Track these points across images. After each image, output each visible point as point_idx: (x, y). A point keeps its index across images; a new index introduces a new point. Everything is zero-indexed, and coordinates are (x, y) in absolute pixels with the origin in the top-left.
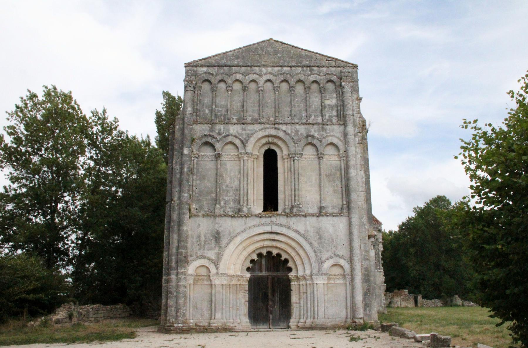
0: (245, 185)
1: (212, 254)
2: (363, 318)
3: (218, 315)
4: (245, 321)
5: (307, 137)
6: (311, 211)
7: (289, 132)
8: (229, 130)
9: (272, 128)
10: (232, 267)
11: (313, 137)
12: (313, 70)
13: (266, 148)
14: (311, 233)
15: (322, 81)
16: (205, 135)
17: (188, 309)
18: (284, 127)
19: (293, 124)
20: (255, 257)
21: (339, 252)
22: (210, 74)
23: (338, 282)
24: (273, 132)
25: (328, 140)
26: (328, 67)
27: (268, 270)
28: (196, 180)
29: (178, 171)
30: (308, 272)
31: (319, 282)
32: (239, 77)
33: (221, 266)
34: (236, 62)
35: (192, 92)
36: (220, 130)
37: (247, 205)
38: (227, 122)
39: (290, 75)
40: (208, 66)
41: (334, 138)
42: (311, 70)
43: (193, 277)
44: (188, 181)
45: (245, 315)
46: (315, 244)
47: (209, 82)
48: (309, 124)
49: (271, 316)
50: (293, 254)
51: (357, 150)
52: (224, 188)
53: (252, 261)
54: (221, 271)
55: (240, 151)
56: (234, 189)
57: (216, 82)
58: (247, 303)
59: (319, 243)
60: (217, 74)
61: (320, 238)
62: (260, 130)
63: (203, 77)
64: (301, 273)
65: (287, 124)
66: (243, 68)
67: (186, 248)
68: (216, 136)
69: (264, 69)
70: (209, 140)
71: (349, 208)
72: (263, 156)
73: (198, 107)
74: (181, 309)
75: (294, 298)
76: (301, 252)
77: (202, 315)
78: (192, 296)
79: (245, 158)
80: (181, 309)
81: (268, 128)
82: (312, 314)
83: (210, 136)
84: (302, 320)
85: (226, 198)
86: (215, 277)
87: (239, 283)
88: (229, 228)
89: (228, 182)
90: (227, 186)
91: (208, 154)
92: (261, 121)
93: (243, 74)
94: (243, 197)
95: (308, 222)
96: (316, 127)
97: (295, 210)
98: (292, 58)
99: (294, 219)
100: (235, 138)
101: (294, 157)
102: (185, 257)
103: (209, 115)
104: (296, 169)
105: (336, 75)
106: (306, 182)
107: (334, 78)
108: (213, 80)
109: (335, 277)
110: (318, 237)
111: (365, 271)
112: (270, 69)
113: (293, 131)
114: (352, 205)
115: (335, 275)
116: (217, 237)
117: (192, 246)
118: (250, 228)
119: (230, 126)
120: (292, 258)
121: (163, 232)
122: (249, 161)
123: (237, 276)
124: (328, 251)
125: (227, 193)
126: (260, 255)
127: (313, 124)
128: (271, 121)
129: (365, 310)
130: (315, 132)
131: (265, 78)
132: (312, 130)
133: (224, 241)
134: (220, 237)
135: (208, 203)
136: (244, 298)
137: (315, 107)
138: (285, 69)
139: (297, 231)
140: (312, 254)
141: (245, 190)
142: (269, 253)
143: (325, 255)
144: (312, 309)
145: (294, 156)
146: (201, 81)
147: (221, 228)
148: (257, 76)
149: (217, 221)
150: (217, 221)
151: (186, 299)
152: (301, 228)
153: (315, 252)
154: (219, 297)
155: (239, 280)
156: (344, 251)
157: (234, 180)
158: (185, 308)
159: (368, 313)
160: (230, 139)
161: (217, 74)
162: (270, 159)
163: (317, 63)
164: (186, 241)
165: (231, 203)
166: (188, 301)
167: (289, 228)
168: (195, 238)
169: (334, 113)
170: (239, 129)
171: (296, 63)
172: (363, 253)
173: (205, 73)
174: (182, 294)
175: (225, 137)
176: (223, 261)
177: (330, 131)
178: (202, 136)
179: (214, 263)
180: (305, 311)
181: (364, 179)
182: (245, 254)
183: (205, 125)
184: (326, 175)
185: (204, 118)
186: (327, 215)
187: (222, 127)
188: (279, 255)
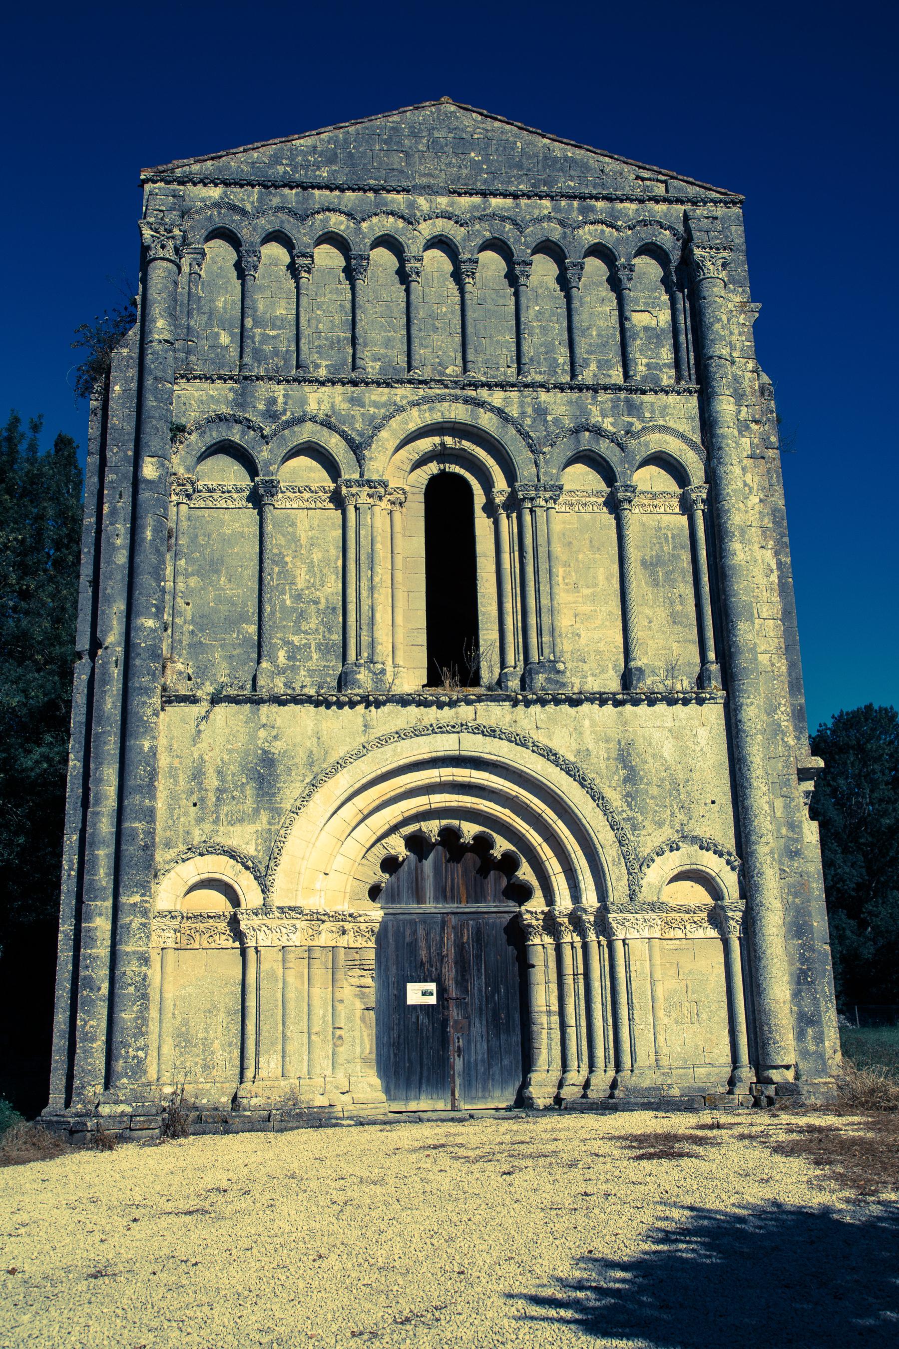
0: (364, 593)
1: (245, 838)
2: (796, 1066)
3: (270, 1065)
4: (367, 1087)
5: (576, 431)
6: (593, 685)
7: (514, 412)
8: (304, 402)
9: (456, 398)
11: (598, 432)
12: (592, 209)
13: (433, 468)
14: (601, 766)
15: (622, 249)
16: (221, 418)
17: (154, 1046)
18: (497, 398)
19: (527, 386)
20: (397, 846)
21: (703, 830)
22: (233, 208)
23: (700, 933)
24: (458, 412)
25: (647, 444)
26: (641, 201)
27: (443, 894)
28: (187, 576)
29: (119, 542)
31: (633, 934)
32: (338, 223)
33: (280, 879)
34: (324, 173)
35: (170, 265)
36: (273, 401)
37: (371, 661)
38: (300, 374)
39: (515, 223)
40: (227, 184)
41: (668, 438)
42: (583, 211)
44: (159, 576)
47: (233, 239)
48: (580, 388)
49: (458, 1064)
51: (749, 478)
52: (288, 602)
53: (390, 864)
54: (278, 899)
55: (345, 476)
56: (322, 606)
57: (257, 239)
59: (628, 795)
60: (260, 212)
61: (631, 777)
62: (414, 404)
63: (210, 218)
64: (564, 903)
65: (502, 386)
66: (349, 194)
67: (150, 815)
68: (256, 419)
69: (422, 201)
70: (236, 435)
71: (729, 680)
72: (422, 498)
73: (192, 323)
74: (126, 1045)
78: (168, 996)
79: (363, 497)
80: (126, 1045)
81: (442, 399)
83: (237, 421)
84: (576, 1077)
85: (296, 639)
86: (256, 921)
87: (343, 941)
88: (308, 744)
89: (301, 583)
90: (298, 597)
91: (229, 484)
92: (417, 374)
93: (350, 215)
94: (358, 636)
95: (587, 723)
96: (602, 397)
97: (540, 679)
98: (520, 166)
100: (326, 431)
101: (532, 499)
102: (146, 848)
103: (234, 353)
104: (542, 540)
105: (670, 228)
106: (576, 586)
107: (665, 238)
108: (245, 233)
109: (687, 916)
110: (623, 772)
111: (796, 895)
112: (443, 201)
113: (529, 410)
114: (743, 661)
116: (264, 773)
117: (171, 809)
118: (382, 741)
119: (307, 388)
121: (66, 761)
122: (377, 509)
124: (660, 824)
125: (297, 622)
126: (416, 843)
127: (594, 389)
128: (447, 375)
129: (800, 1036)
130: (604, 415)
131: (426, 230)
132: (595, 410)
133: (290, 791)
135: (231, 657)
136: (362, 996)
137: (599, 335)
138: (496, 202)
141: (365, 608)
142: (450, 836)
143: (650, 839)
145: (533, 493)
146: (204, 233)
147: (278, 743)
148: (401, 224)
150: (264, 720)
151: (145, 1008)
152: (563, 743)
154: (271, 994)
156: (721, 830)
157: (323, 575)
158: (141, 1043)
159: (812, 1048)
160: (307, 432)
161: (260, 212)
162: (448, 515)
163: (603, 185)
164: (150, 790)
165: (315, 656)
166: (153, 1013)
167: (521, 742)
168: (182, 778)
169: (666, 354)
170: (338, 399)
171: (533, 185)
172: (784, 831)
173: (217, 205)
174: (131, 989)
175: (289, 424)
177: (653, 412)
178: (209, 421)
181: (774, 578)
182: (366, 834)
183: (219, 384)
184: (644, 563)
185: (213, 362)
187: (279, 391)
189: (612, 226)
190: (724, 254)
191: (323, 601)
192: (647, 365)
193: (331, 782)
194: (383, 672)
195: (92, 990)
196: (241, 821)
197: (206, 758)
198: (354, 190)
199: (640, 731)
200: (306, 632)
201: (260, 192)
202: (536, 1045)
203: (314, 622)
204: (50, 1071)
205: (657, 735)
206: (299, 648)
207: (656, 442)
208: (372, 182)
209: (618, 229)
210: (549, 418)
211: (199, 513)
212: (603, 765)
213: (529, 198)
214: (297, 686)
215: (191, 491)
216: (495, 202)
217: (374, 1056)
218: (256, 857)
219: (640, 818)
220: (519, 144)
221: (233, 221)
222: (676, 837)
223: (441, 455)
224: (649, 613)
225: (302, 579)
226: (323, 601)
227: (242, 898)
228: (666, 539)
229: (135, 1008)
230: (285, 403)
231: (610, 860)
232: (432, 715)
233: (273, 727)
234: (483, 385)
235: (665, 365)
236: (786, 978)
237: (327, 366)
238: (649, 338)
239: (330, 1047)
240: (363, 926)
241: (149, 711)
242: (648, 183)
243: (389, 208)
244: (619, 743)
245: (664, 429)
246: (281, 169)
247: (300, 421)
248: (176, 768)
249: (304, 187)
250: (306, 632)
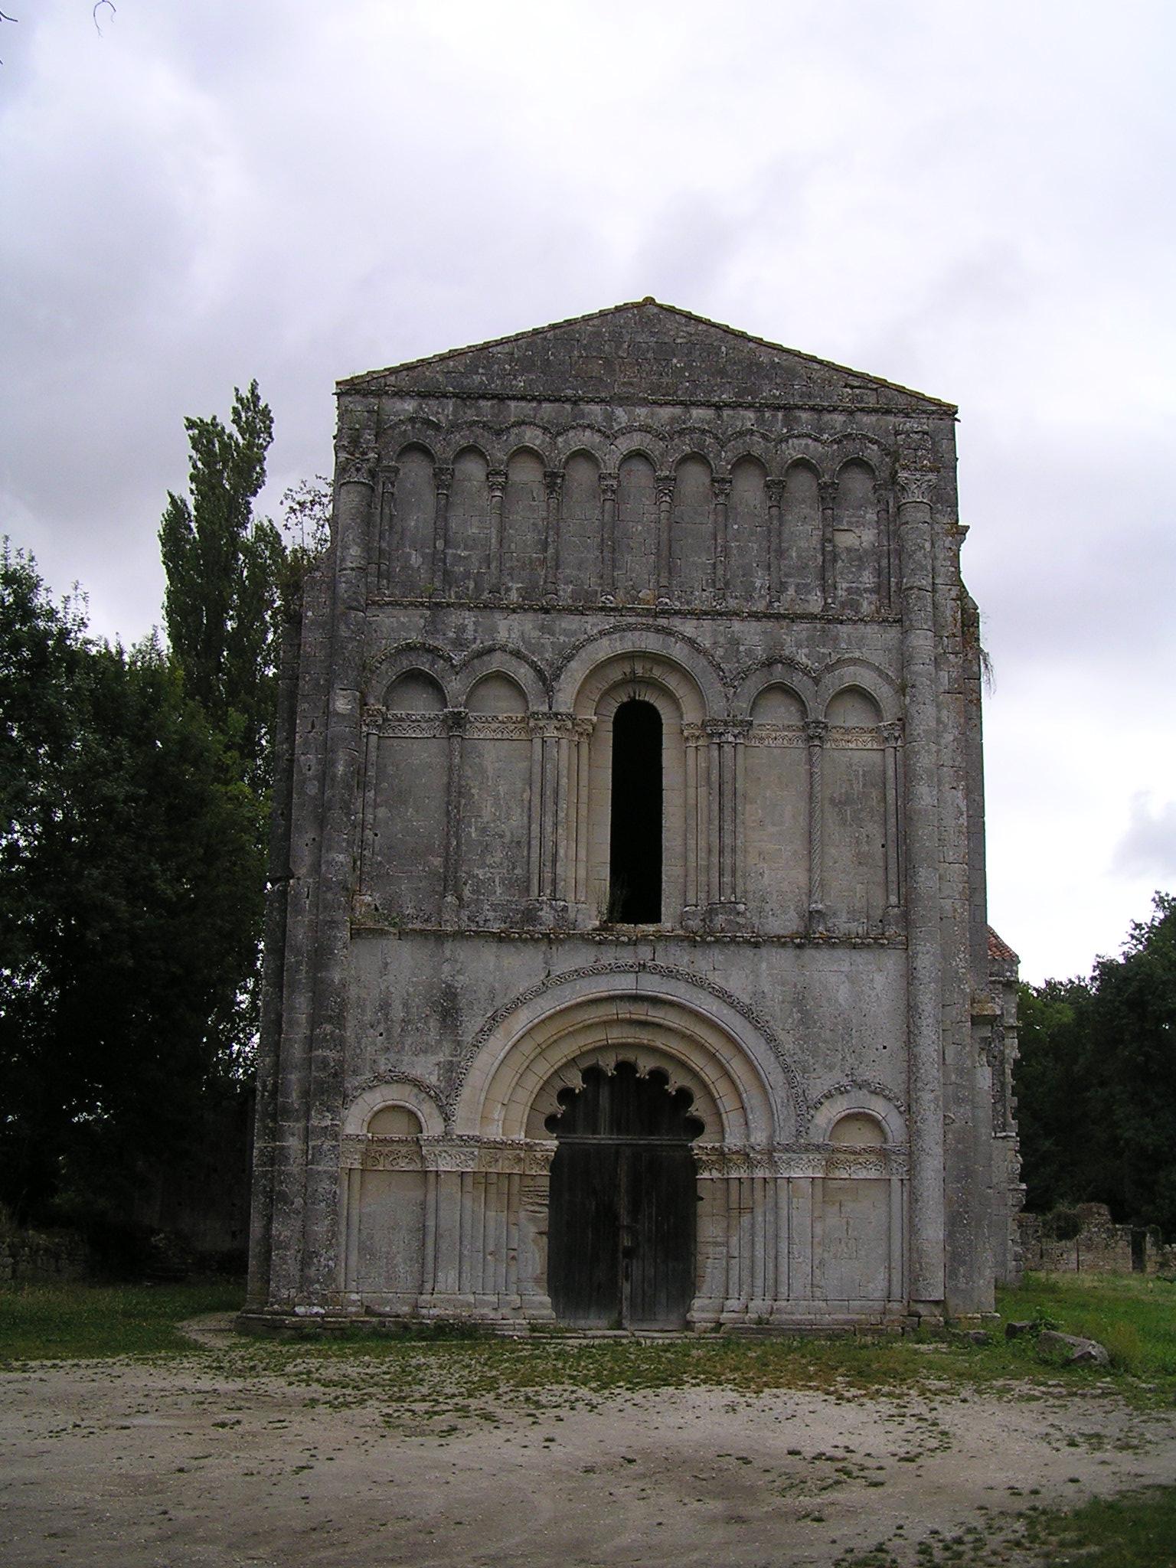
1: (427, 1069)
3: (448, 1278)
5: (769, 663)
8: (493, 630)
9: (648, 628)
10: (498, 1113)
11: (791, 664)
16: (410, 648)
18: (688, 628)
20: (577, 1082)
22: (428, 423)
24: (651, 642)
27: (618, 1125)
30: (759, 1138)
32: (533, 437)
36: (462, 629)
40: (423, 396)
42: (787, 423)
43: (362, 1147)
45: (537, 1280)
46: (787, 1041)
48: (779, 617)
49: (626, 1288)
50: (710, 1074)
53: (566, 1095)
54: (460, 1129)
56: (506, 840)
57: (451, 455)
58: (545, 1239)
60: (455, 426)
61: (806, 1019)
62: (603, 633)
75: (709, 1229)
76: (736, 1067)
77: (389, 1278)
81: (630, 628)
82: (771, 1282)
90: (483, 830)
95: (764, 965)
99: (717, 955)
100: (514, 661)
108: (437, 449)
109: (853, 1157)
110: (797, 1016)
115: (854, 1153)
118: (562, 979)
119: (498, 616)
120: (705, 1086)
123: (514, 1145)
124: (831, 1068)
126: (593, 1075)
131: (624, 445)
133: (472, 1024)
134: (458, 1010)
137: (799, 557)
139: (723, 996)
140: (774, 1076)
142: (626, 1068)
144: (771, 1266)
149: (448, 953)
151: (335, 1222)
152: (737, 983)
153: (786, 1069)
155: (520, 1160)
156: (884, 1070)
158: (332, 1253)
161: (455, 426)
162: (637, 739)
165: (499, 891)
171: (737, 395)
173: (412, 420)
175: (480, 654)
176: (466, 1092)
177: (849, 643)
179: (436, 1098)
180: (745, 1274)
182: (544, 1069)
186: (830, 942)
187: (469, 619)
188: (659, 1077)
189: (816, 440)
190: (931, 476)
191: (508, 834)
192: (848, 589)
193: (512, 1018)
194: (565, 909)
195: (286, 1204)
196: (425, 1052)
197: (392, 989)
198: (551, 401)
199: (816, 975)
200: (490, 866)
201: (455, 405)
202: (700, 1272)
203: (498, 856)
204: (661, 790)
205: (833, 979)
206: (483, 882)
207: (853, 675)
208: (569, 392)
209: (823, 443)
210: (742, 648)
211: (388, 742)
212: (777, 1008)
213: (733, 408)
214: (480, 919)
215: (380, 722)
216: (696, 412)
217: (545, 1276)
218: (438, 1087)
219: (811, 1061)
220: (723, 349)
221: (428, 437)
222: (845, 1081)
223: (632, 680)
224: (839, 852)
225: (488, 811)
226: (508, 834)
227: (424, 1125)
228: (857, 776)
229: (327, 1222)
230: (476, 631)
231: (779, 1101)
232: (609, 956)
233: (456, 961)
234: (677, 613)
235: (866, 590)
236: (941, 1220)
237: (518, 589)
238: (851, 560)
239: (501, 1270)
240: (538, 1155)
241: (340, 944)
242: (858, 391)
243: (586, 422)
244: (795, 986)
245: (855, 661)
246: (477, 378)
247: (490, 650)
248: (365, 1000)
249: (501, 398)
250: (490, 866)
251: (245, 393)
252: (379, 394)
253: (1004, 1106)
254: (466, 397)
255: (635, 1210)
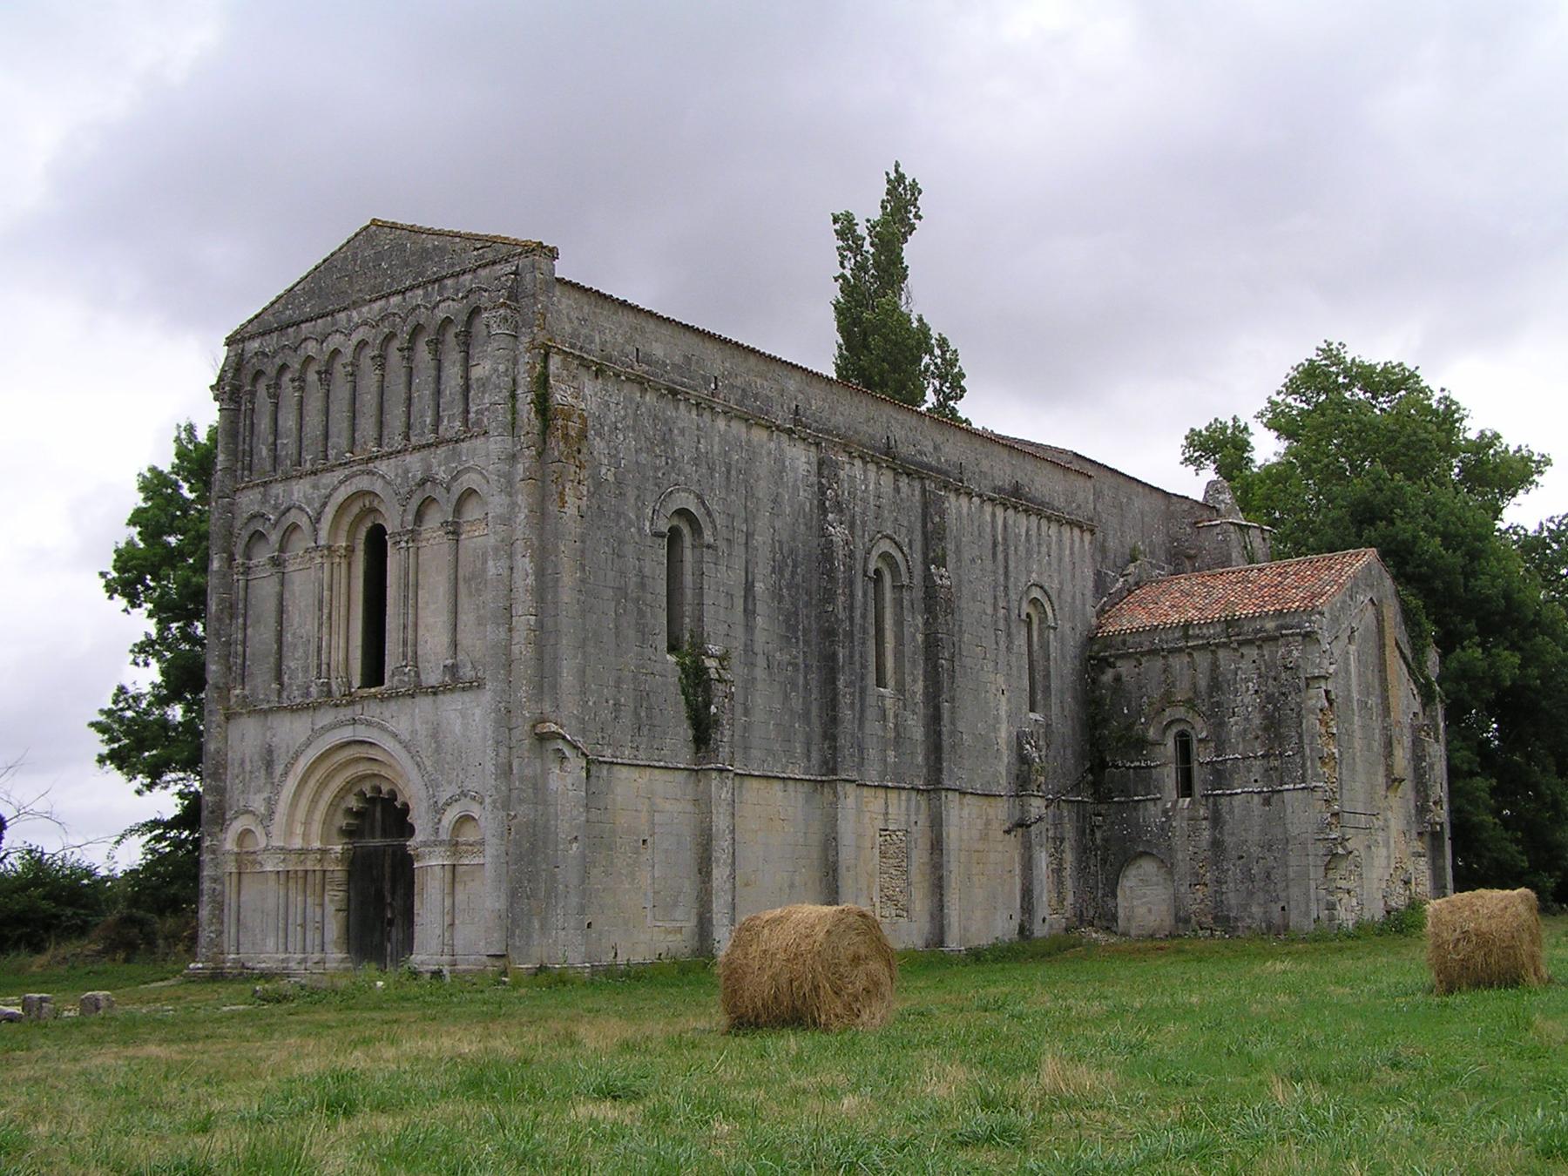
5: (423, 483)
62: (341, 483)
81: (354, 475)
133: (279, 769)
247: (289, 509)
251: (893, 175)
252: (243, 340)
253: (1303, 757)
254: (282, 328)
255: (393, 893)
